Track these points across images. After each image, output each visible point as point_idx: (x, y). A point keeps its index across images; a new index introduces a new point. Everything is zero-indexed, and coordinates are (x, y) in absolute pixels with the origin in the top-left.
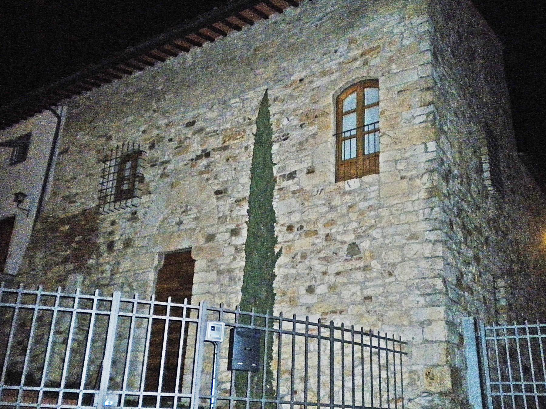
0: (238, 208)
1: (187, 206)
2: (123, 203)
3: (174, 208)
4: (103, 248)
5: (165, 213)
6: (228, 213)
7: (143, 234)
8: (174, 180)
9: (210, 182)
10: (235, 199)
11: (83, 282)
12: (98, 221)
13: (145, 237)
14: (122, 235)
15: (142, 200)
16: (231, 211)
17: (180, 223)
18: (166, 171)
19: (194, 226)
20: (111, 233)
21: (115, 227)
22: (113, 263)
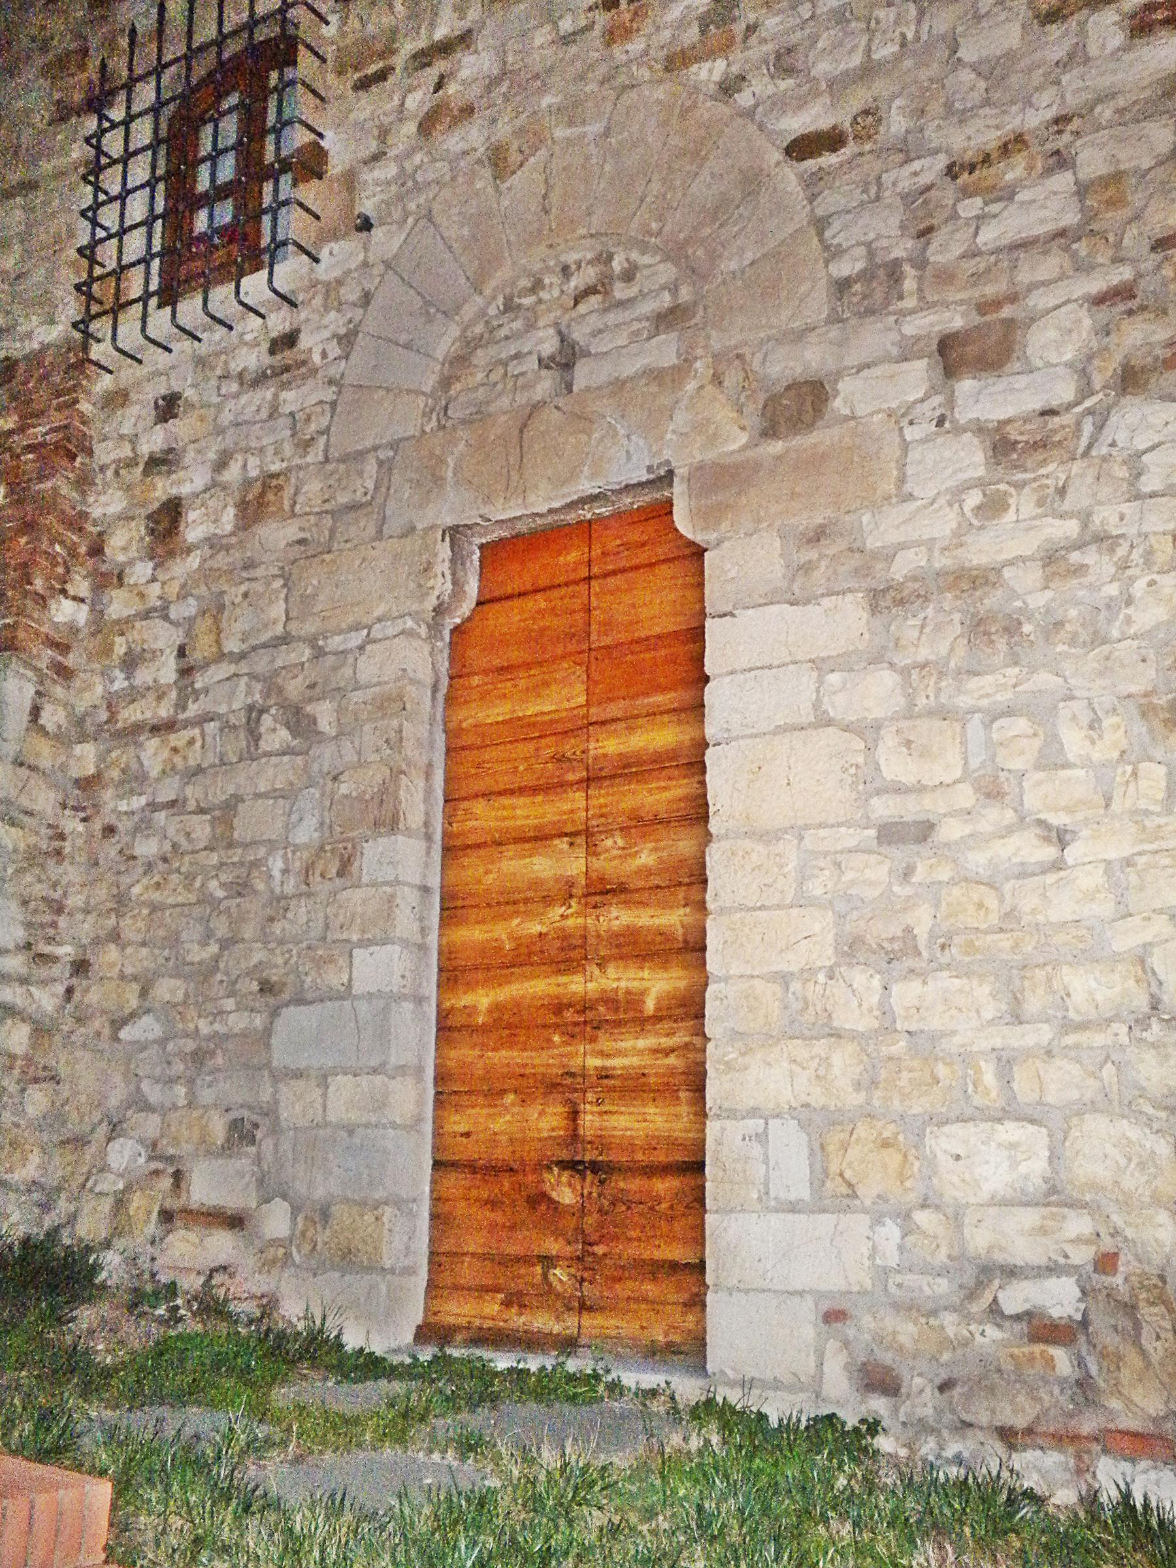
0: (971, 207)
1: (606, 259)
2: (221, 295)
3: (525, 283)
4: (124, 543)
5: (468, 312)
6: (902, 248)
7: (342, 442)
8: (503, 130)
9: (744, 99)
10: (942, 161)
11: (36, 712)
12: (85, 407)
13: (361, 455)
14: (221, 464)
15: (321, 268)
16: (926, 233)
17: (565, 360)
18: (452, 89)
19: (669, 358)
20: (162, 462)
21: (181, 427)
22: (190, 608)
